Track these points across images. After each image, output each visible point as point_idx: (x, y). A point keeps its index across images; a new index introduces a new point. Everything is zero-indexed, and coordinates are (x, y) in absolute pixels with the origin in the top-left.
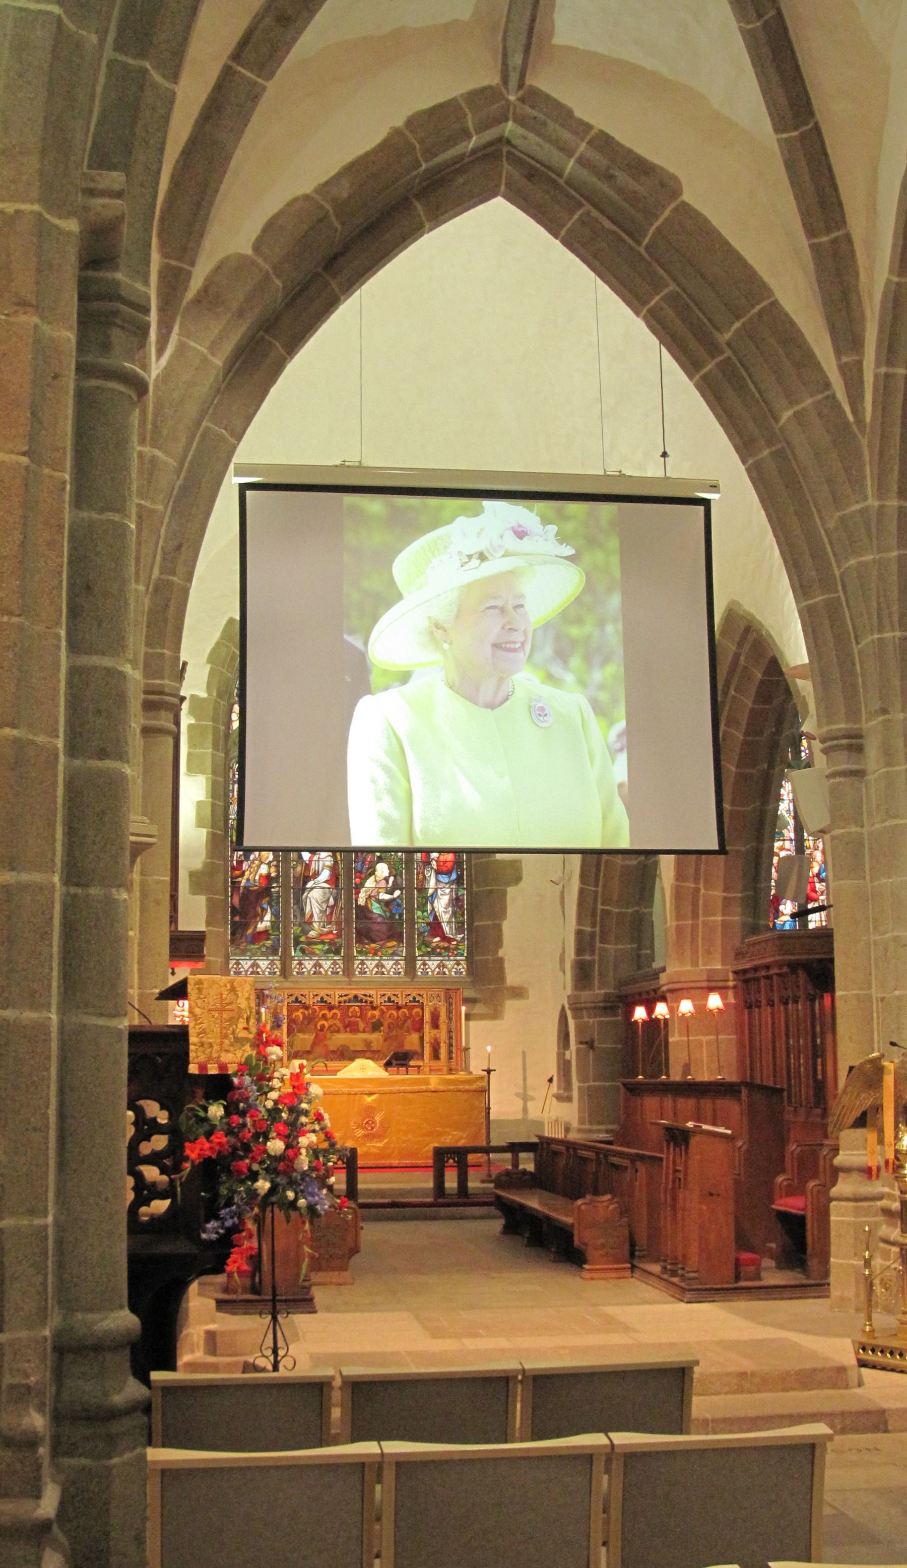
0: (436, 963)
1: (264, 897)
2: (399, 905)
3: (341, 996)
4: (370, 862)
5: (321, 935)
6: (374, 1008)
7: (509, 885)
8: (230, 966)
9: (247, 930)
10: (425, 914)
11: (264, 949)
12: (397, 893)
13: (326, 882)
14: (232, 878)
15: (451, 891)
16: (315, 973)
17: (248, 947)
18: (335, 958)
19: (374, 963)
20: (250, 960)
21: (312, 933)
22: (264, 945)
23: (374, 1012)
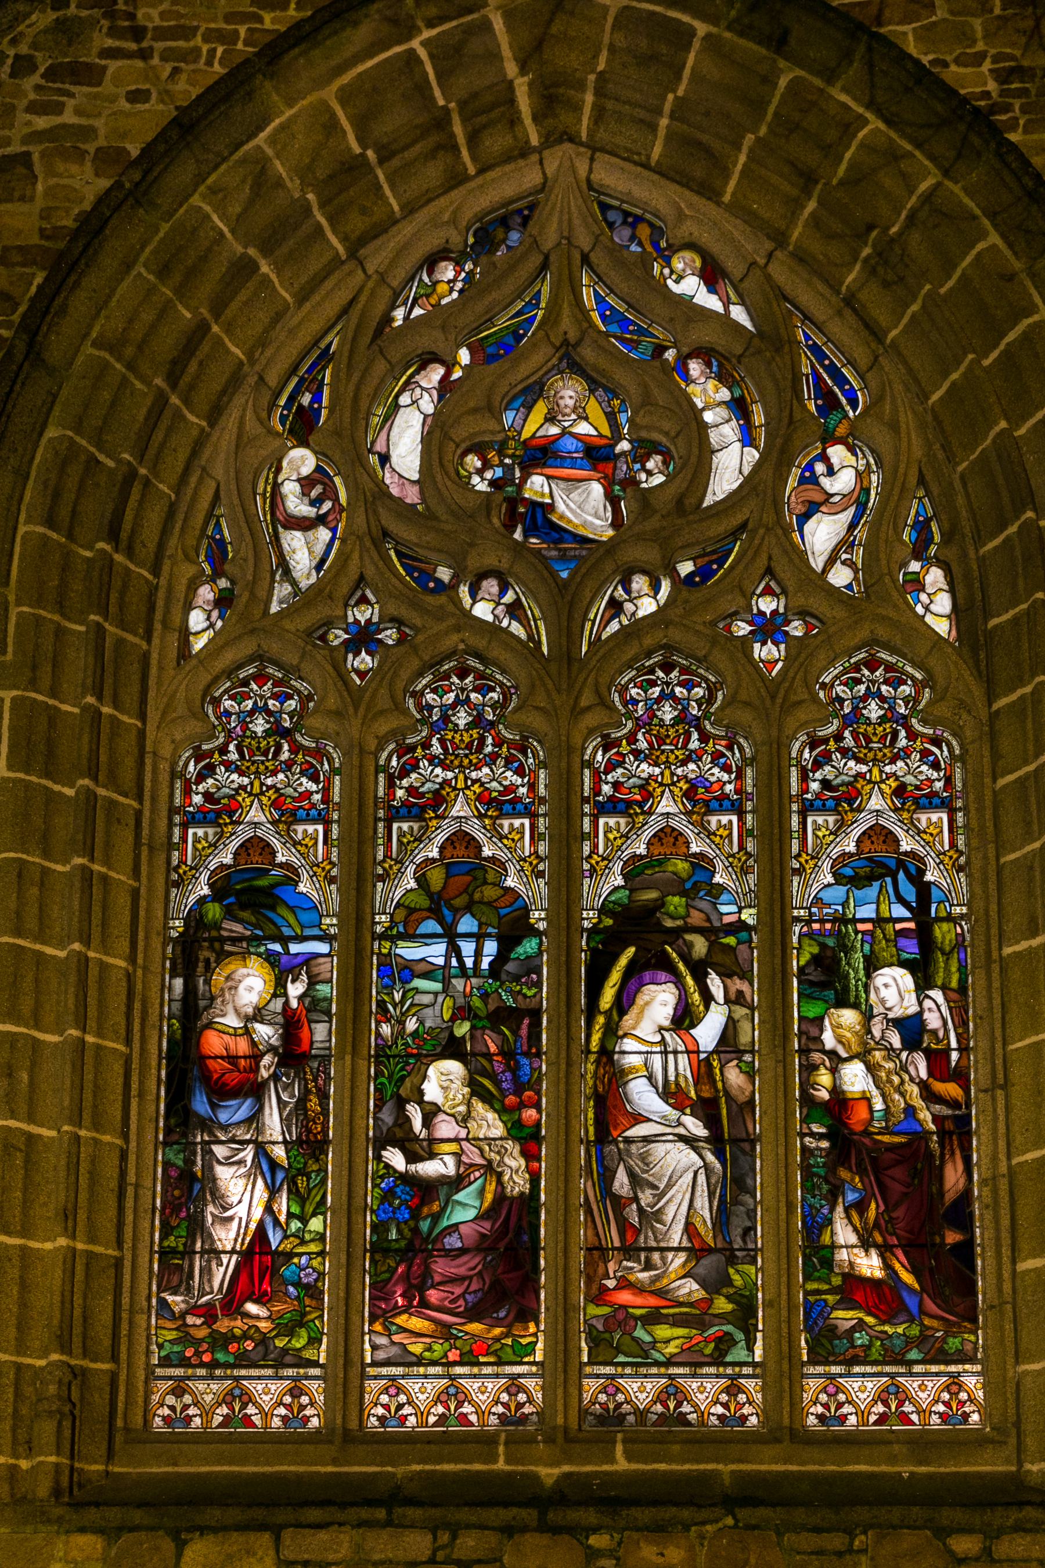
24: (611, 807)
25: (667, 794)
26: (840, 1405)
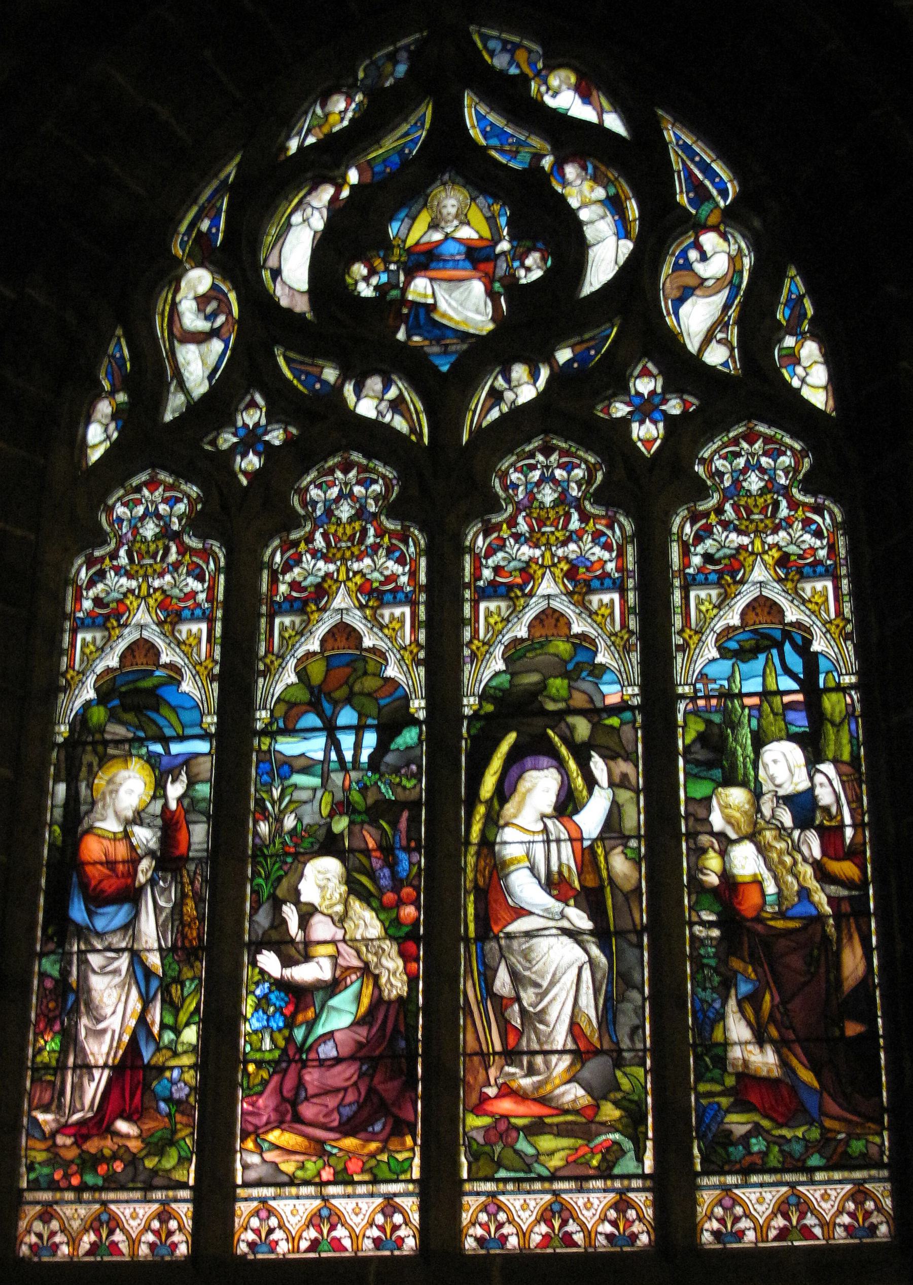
20: (372, 1195)
24: (493, 591)
25: (548, 575)
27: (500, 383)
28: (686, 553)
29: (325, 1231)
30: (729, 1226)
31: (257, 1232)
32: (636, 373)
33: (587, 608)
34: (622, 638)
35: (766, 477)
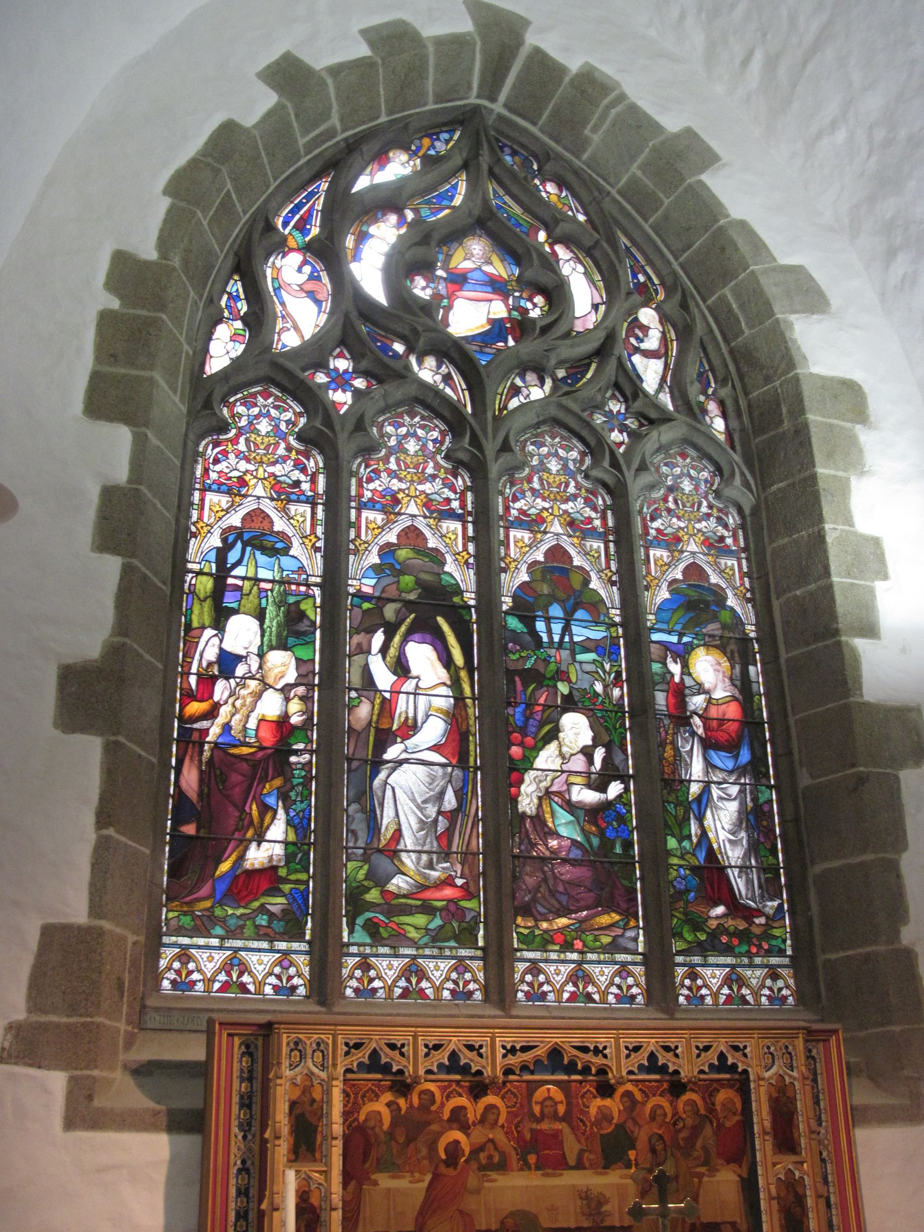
0: (720, 973)
1: (265, 779)
2: (622, 820)
3: (513, 1051)
4: (546, 707)
5: (423, 888)
6: (606, 1090)
7: (902, 765)
8: (163, 963)
9: (219, 861)
10: (686, 844)
11: (263, 920)
12: (615, 789)
13: (435, 748)
14: (181, 719)
15: (742, 792)
16: (406, 993)
17: (218, 912)
18: (463, 952)
19: (566, 969)
20: (221, 948)
21: (399, 883)
22: (263, 909)
23: (608, 1102)
24: (371, 504)
25: (412, 502)
26: (371, 980)
27: (518, 382)
28: (360, 485)
29: (581, 987)
30: (184, 976)
31: (530, 984)
32: (335, 353)
33: (287, 514)
34: (311, 540)
35: (273, 423)
